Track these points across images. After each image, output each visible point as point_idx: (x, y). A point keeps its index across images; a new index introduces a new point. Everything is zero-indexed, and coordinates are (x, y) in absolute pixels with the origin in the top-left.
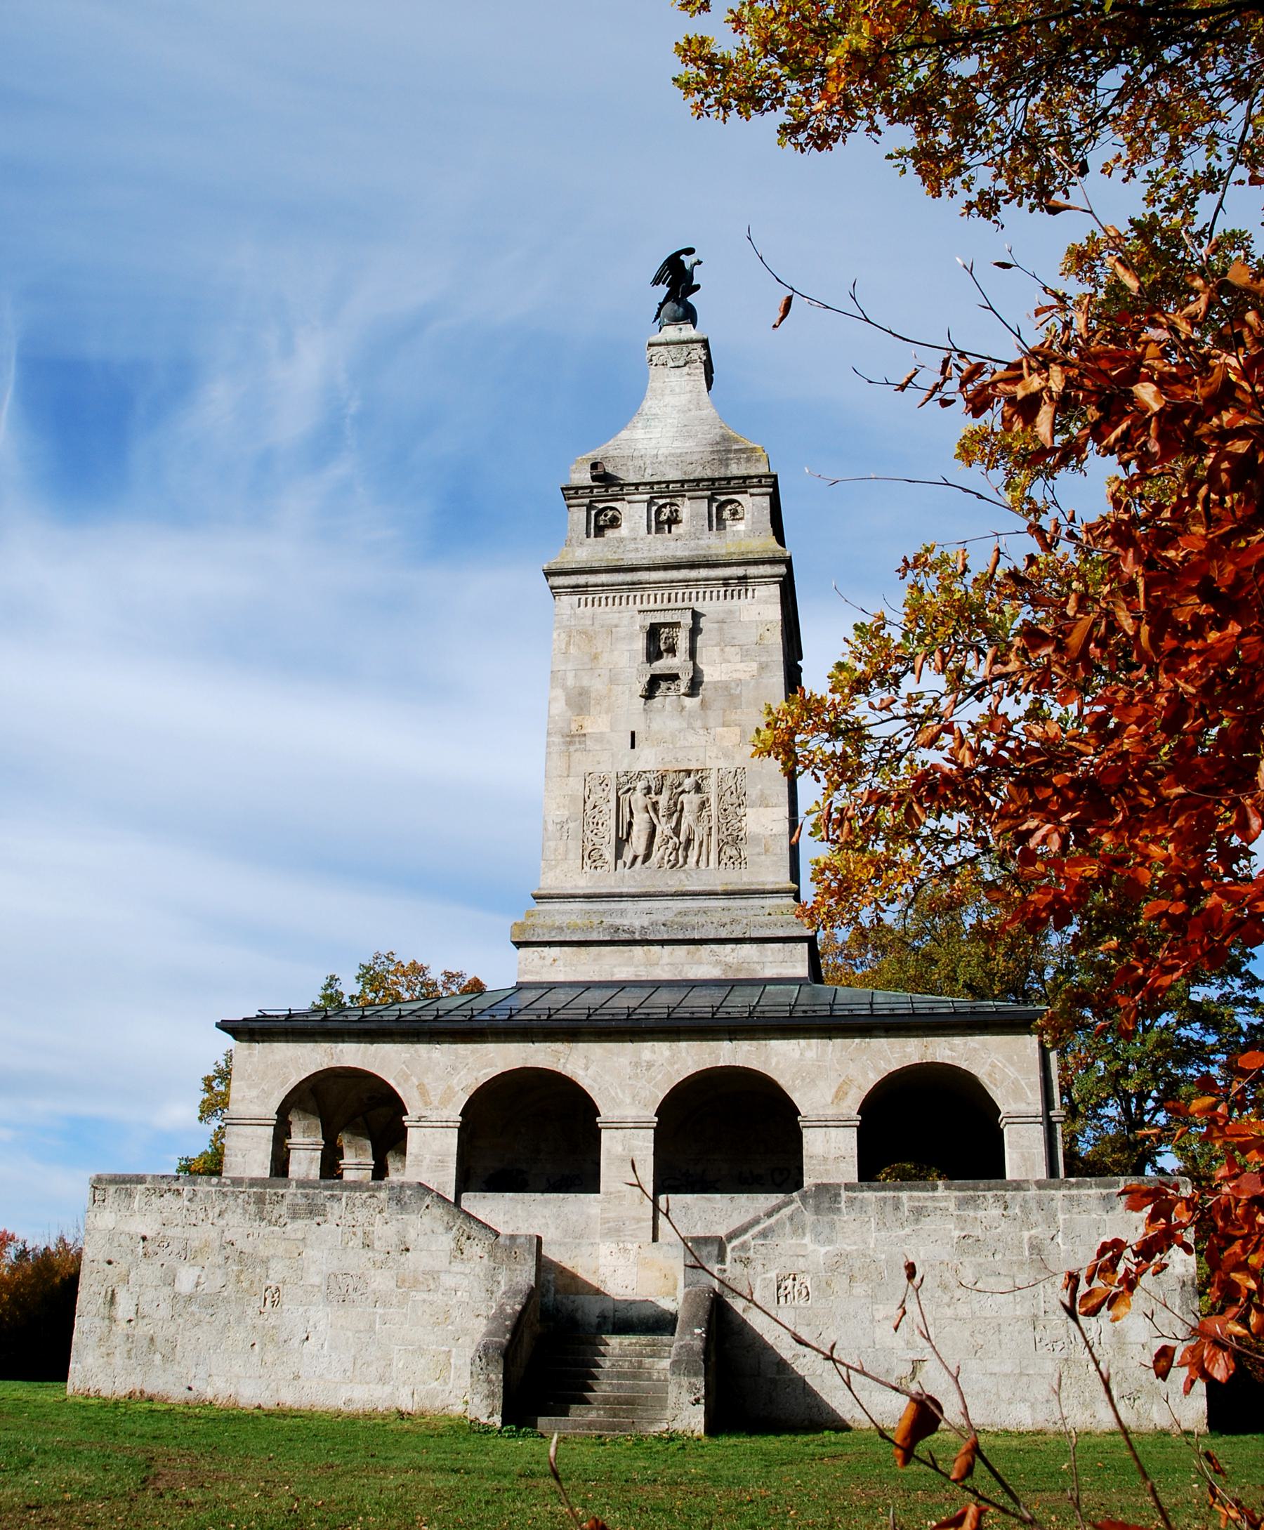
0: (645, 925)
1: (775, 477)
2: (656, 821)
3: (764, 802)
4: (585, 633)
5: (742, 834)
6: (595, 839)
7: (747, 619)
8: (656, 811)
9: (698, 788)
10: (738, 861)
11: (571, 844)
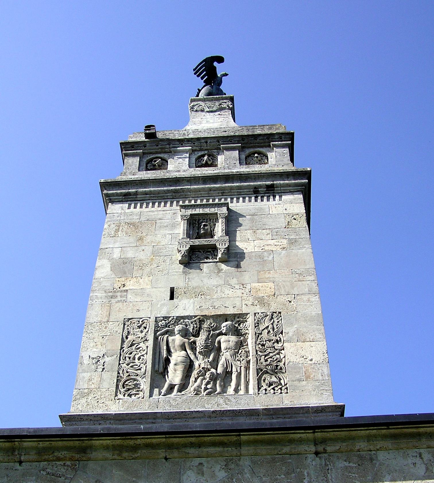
1: (307, 175)
2: (192, 357)
3: (300, 338)
5: (281, 364)
8: (193, 348)
9: (237, 332)
10: (278, 386)
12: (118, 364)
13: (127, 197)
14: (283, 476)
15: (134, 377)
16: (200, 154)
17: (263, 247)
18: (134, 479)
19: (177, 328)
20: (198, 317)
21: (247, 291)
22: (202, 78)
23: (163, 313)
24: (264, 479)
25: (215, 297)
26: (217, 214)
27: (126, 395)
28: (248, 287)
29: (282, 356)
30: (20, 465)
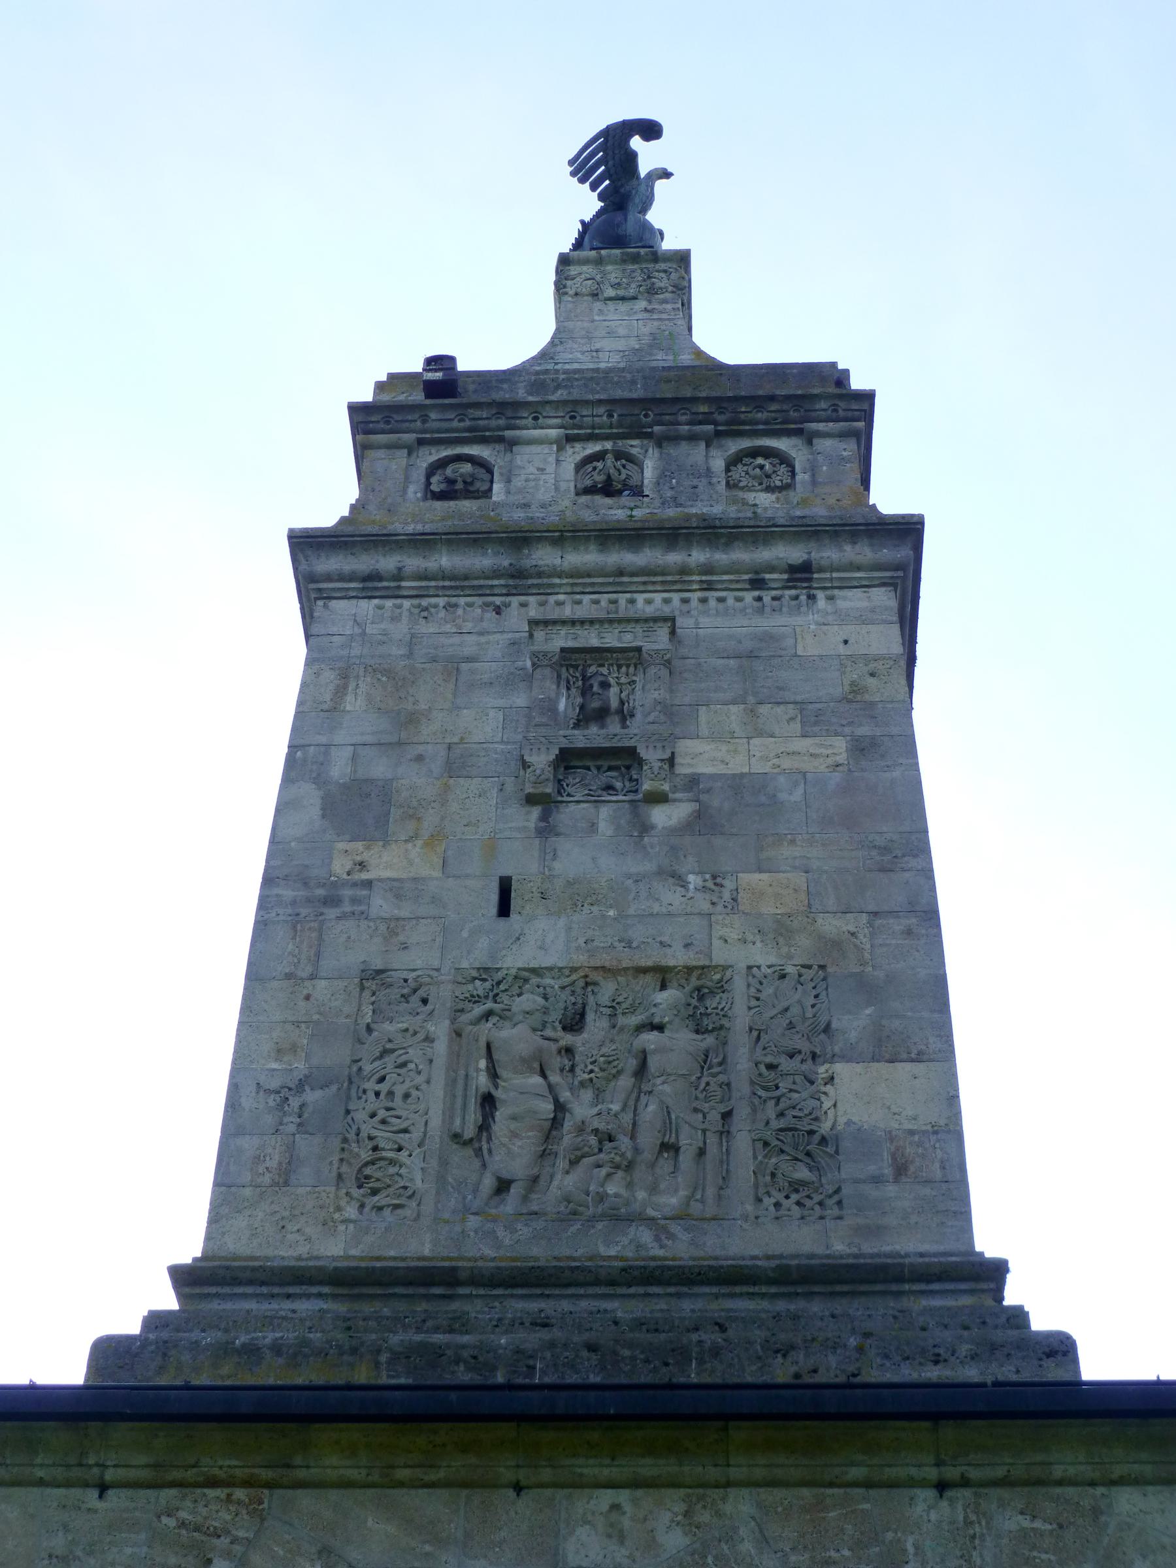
4: (388, 672)
6: (383, 1137)
7: (813, 651)
12: (342, 1112)
13: (370, 584)
14: (846, 1553)
16: (589, 451)
17: (776, 761)
18: (428, 1548)
21: (727, 895)
22: (593, 187)
23: (478, 956)
24: (793, 1558)
25: (631, 911)
26: (639, 649)
27: (367, 1209)
28: (729, 884)
29: (827, 1104)
30: (100, 1497)
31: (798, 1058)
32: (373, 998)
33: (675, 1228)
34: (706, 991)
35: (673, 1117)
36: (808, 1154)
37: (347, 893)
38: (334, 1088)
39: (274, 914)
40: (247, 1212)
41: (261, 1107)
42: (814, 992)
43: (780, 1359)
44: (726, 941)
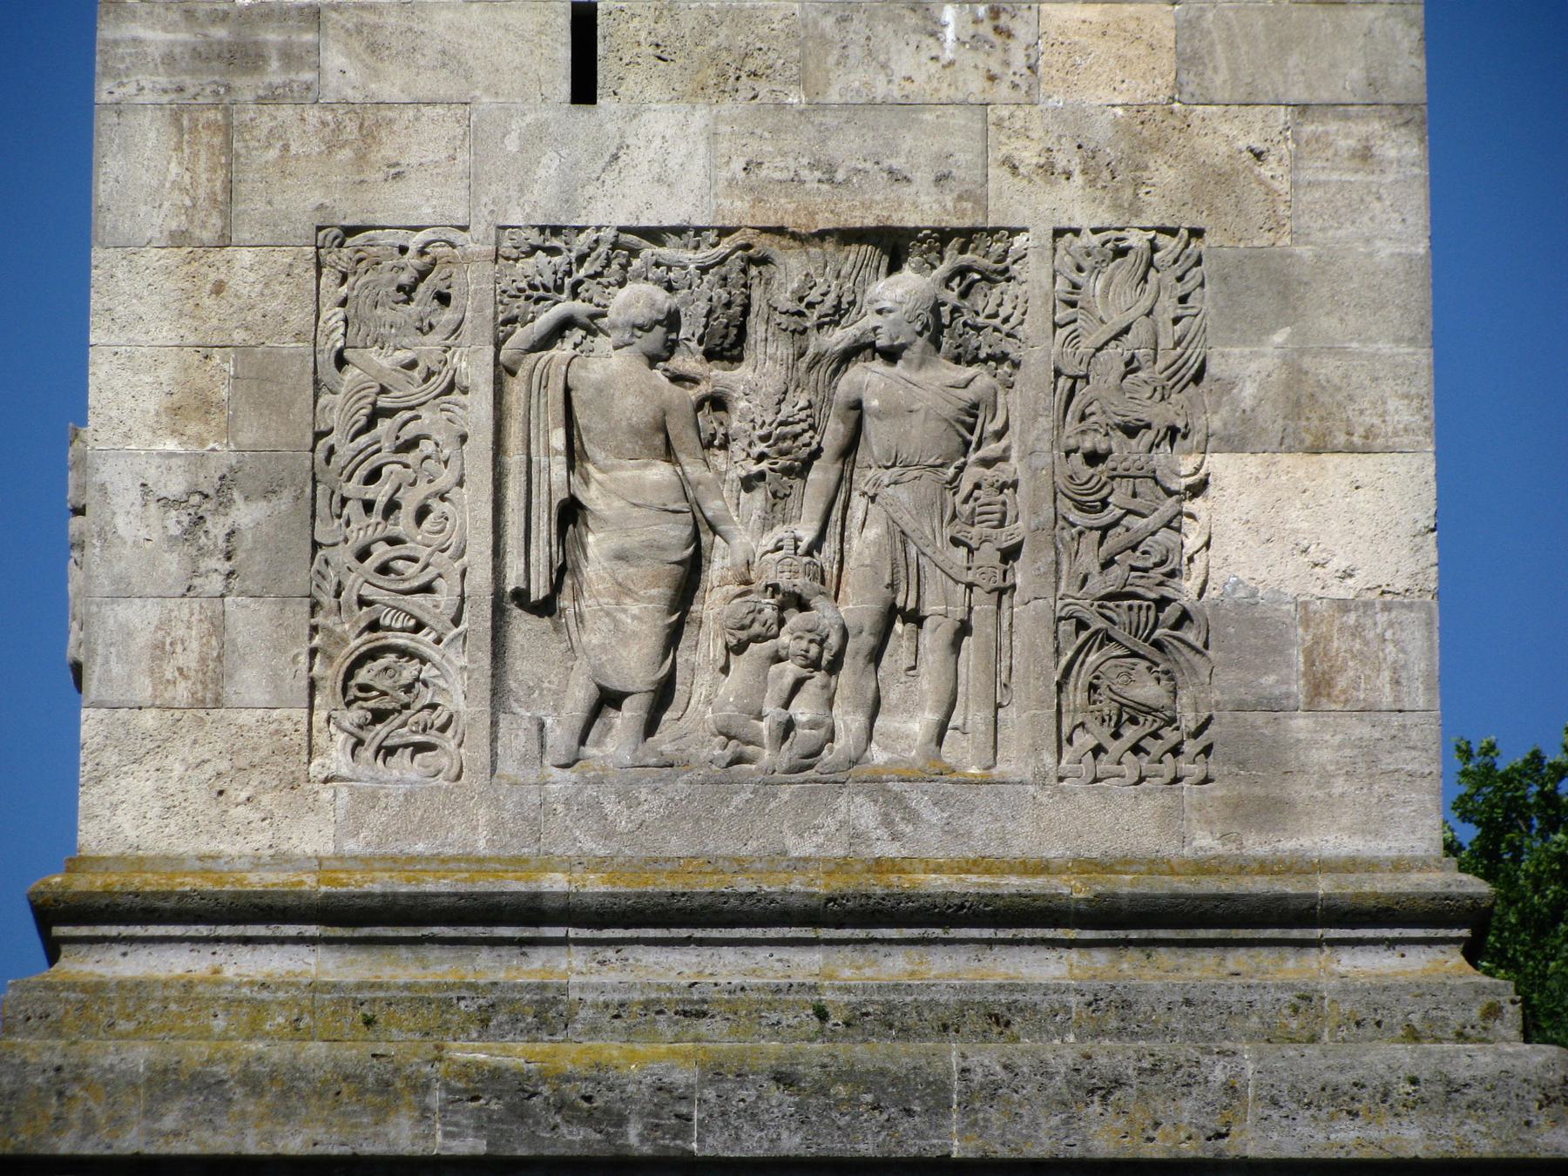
0: (682, 1076)
3: (1310, 424)
11: (249, 619)
15: (402, 640)
19: (634, 299)
20: (738, 238)
21: (1019, 61)
29: (1193, 542)
31: (1147, 437)
32: (344, 290)
33: (918, 798)
34: (977, 276)
35: (913, 551)
36: (1158, 645)
37: (272, 36)
38: (287, 495)
39: (131, 89)
40: (152, 763)
41: (155, 536)
42: (1180, 290)
43: (1096, 1108)
44: (1015, 167)
